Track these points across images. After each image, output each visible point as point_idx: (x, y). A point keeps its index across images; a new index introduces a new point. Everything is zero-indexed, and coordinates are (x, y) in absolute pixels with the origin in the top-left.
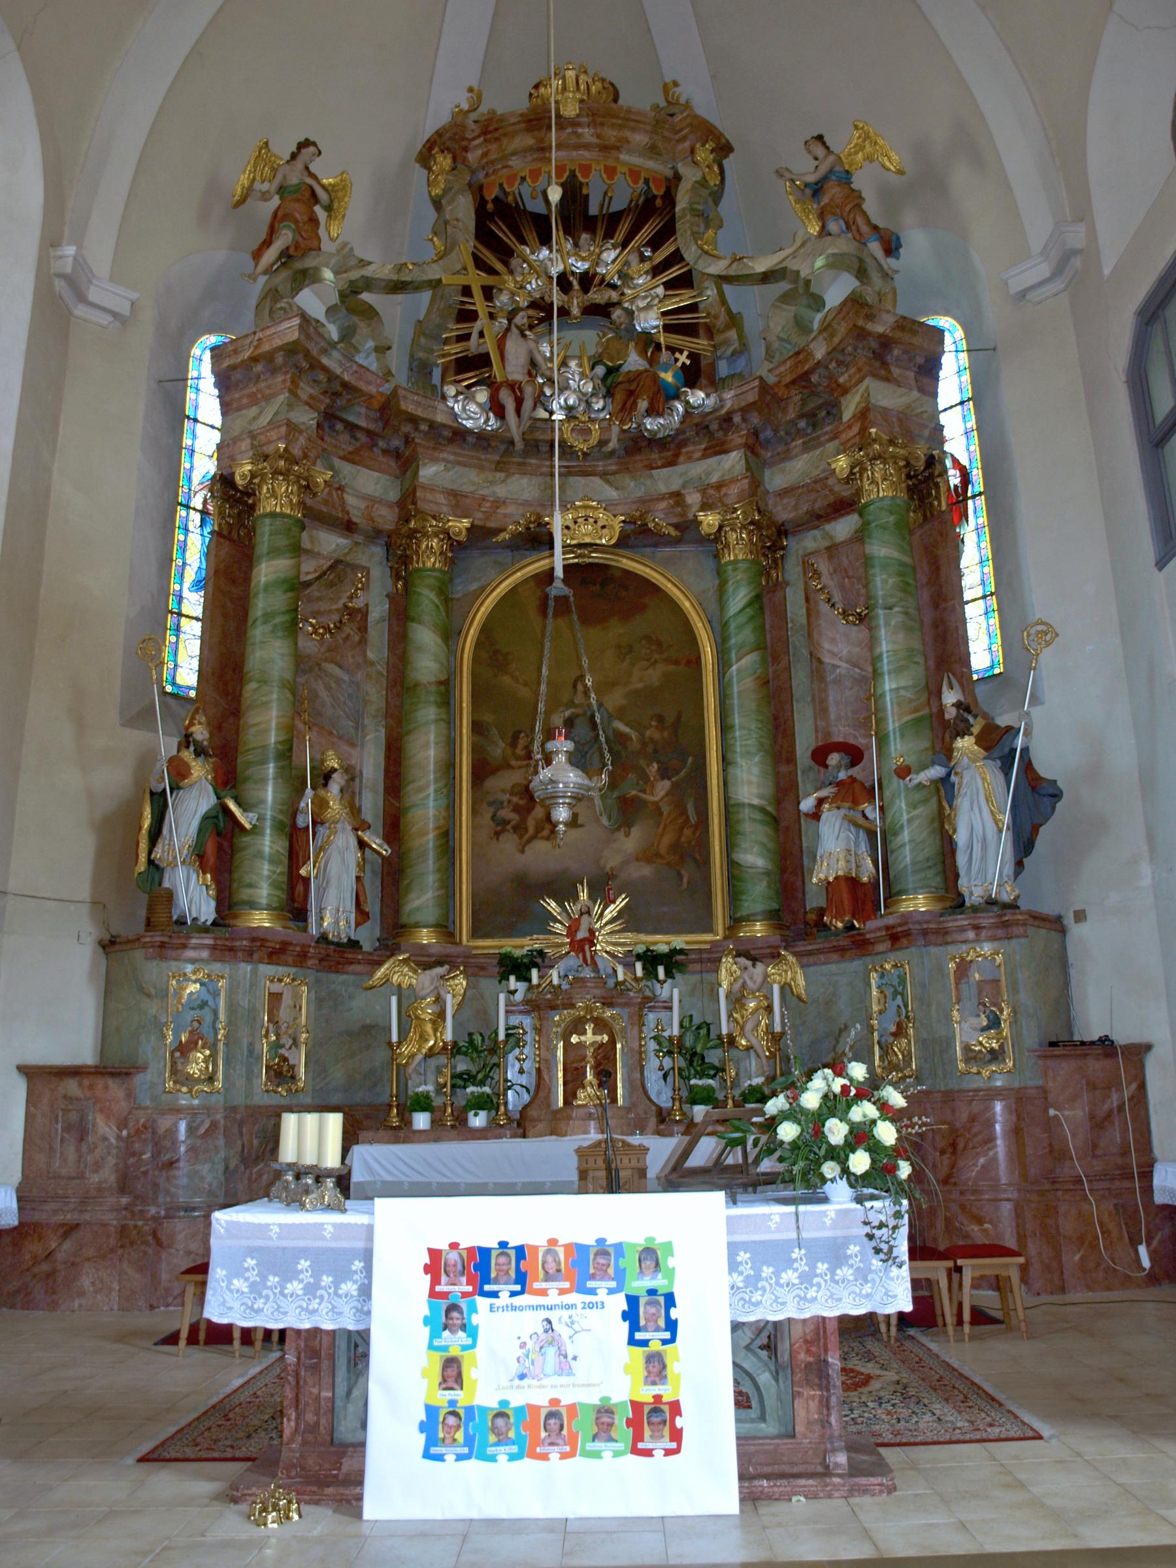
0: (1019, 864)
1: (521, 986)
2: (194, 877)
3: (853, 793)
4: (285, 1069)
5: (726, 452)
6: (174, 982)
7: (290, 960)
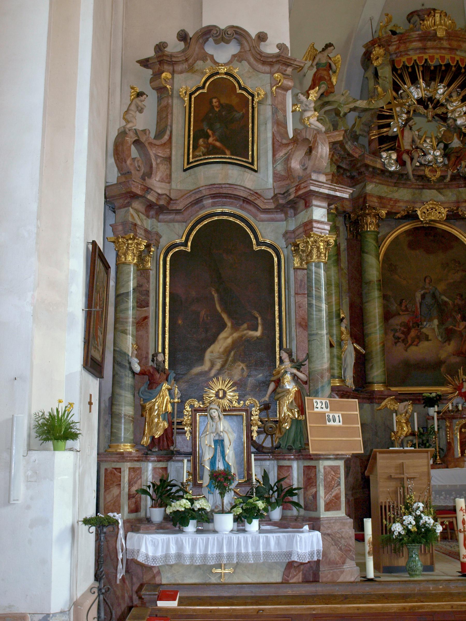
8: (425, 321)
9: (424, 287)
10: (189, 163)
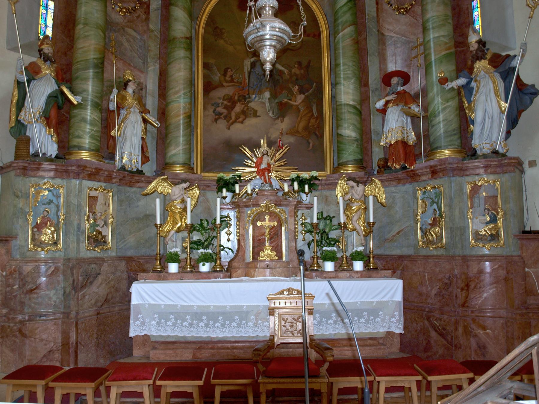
0: (508, 133)
1: (229, 195)
2: (44, 130)
3: (404, 99)
4: (100, 237)
6: (33, 189)
7: (102, 179)
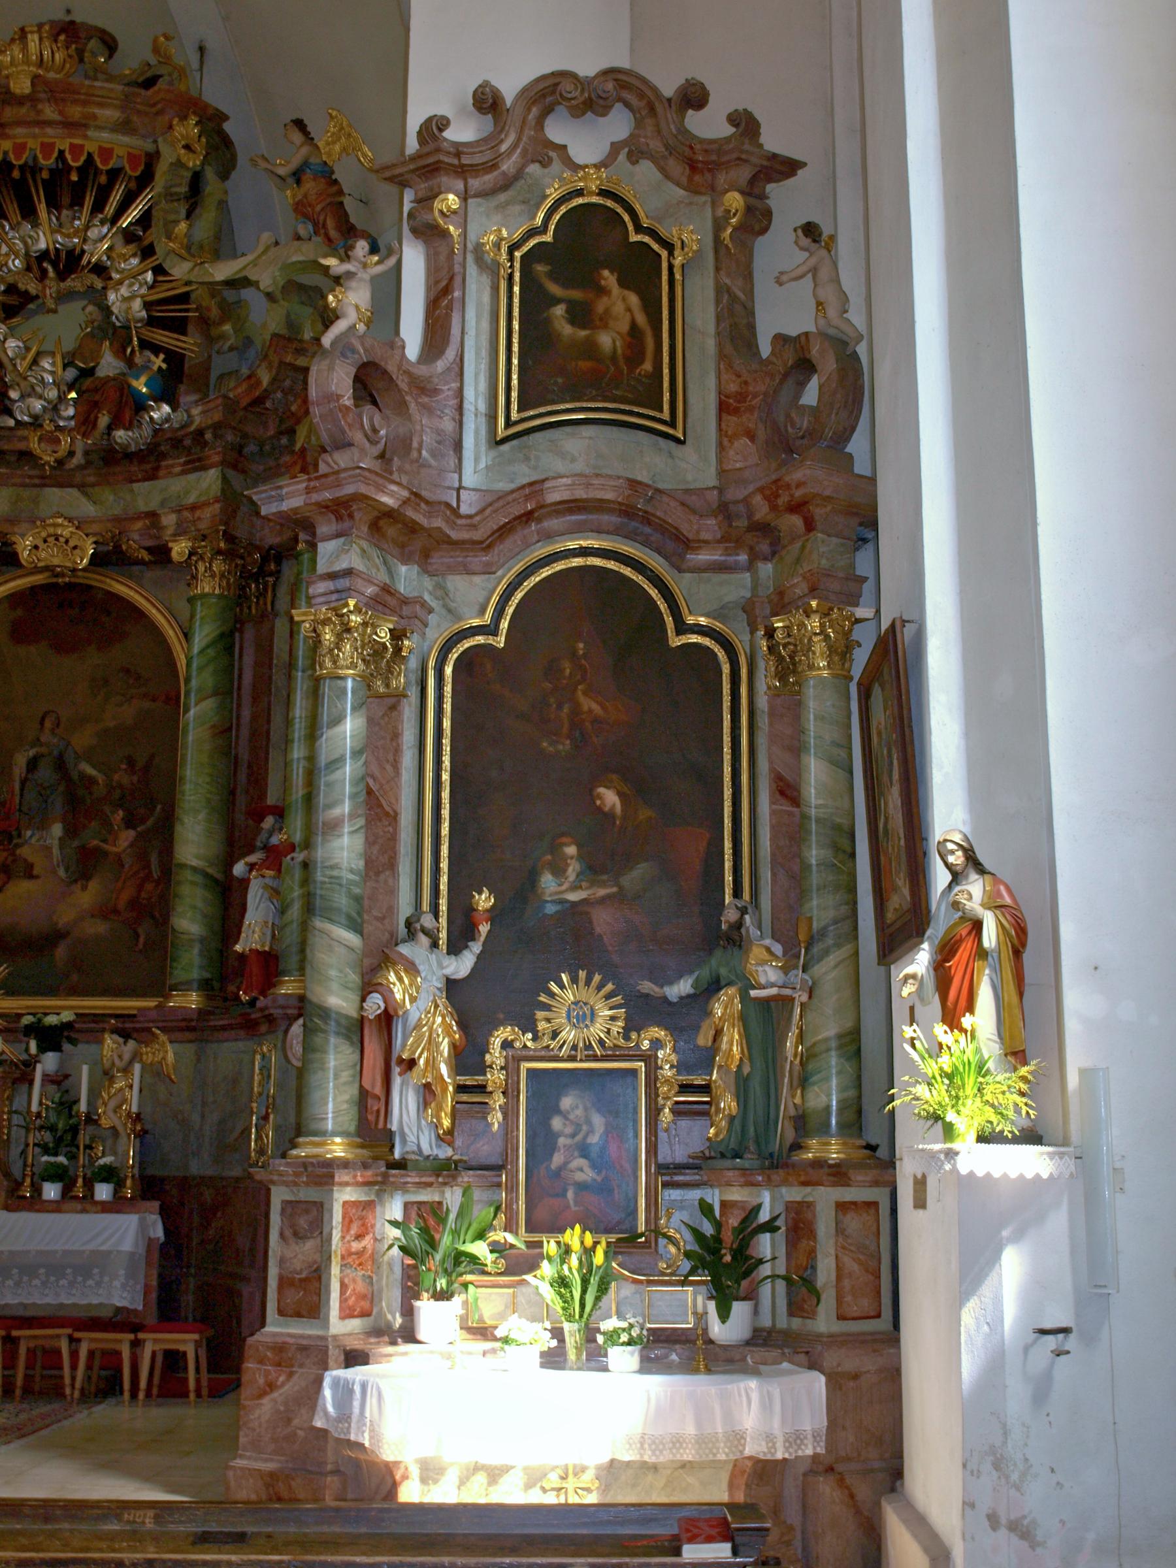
5: (204, 468)
8: (27, 828)
9: (38, 740)
10: (509, 423)
